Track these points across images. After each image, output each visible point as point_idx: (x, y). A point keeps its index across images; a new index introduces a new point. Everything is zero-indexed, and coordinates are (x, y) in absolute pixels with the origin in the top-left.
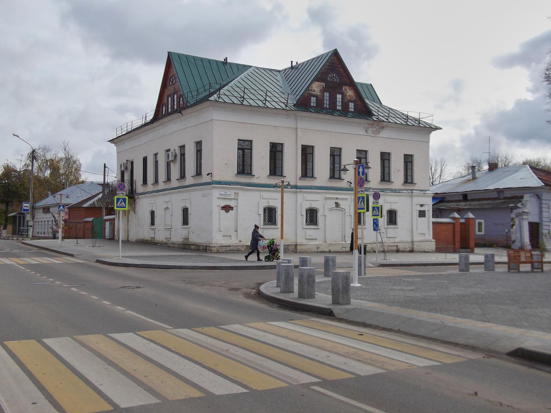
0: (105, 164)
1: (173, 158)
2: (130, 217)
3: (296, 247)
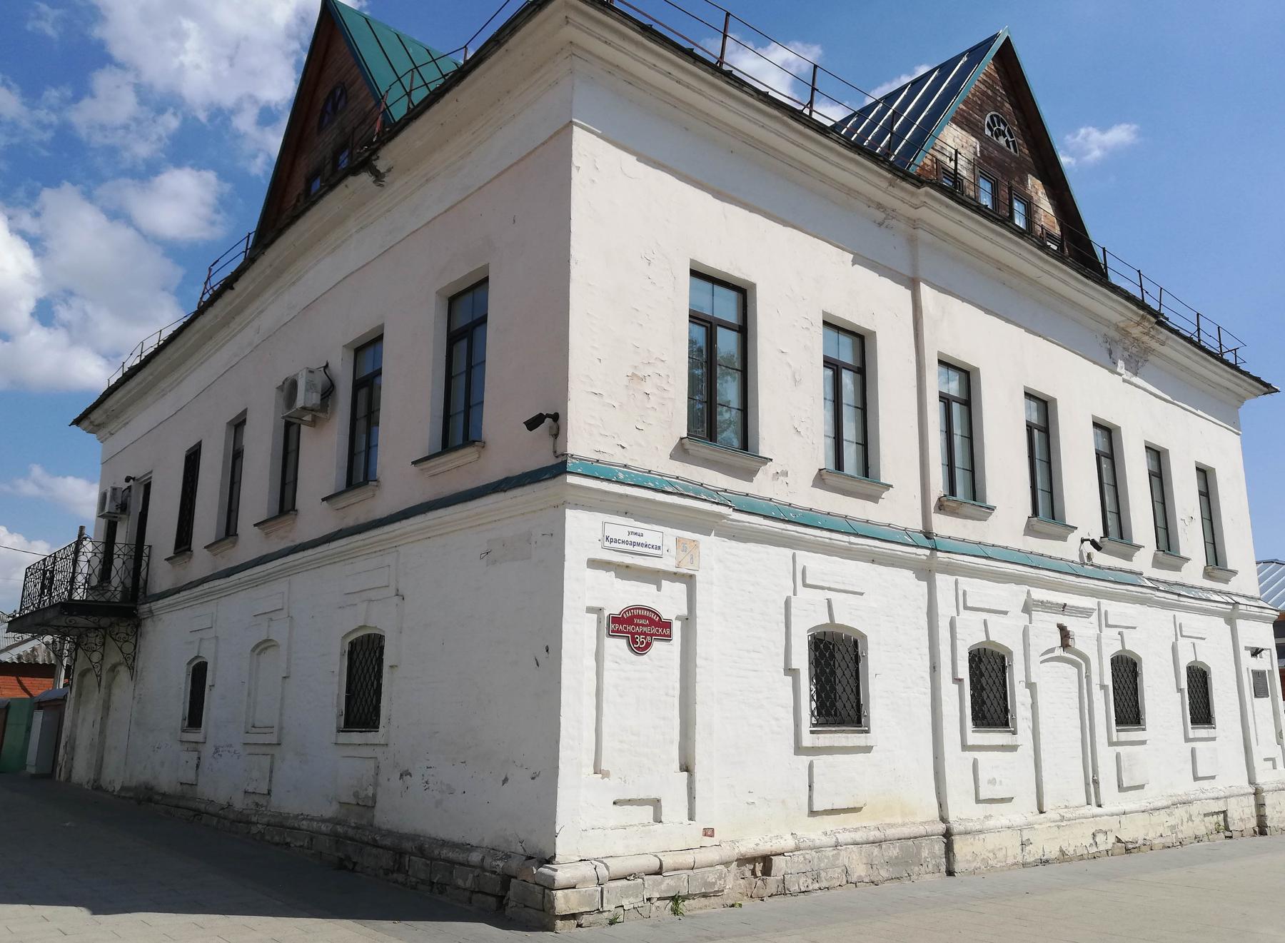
0: (82, 528)
1: (315, 399)
2: (116, 692)
3: (949, 848)
